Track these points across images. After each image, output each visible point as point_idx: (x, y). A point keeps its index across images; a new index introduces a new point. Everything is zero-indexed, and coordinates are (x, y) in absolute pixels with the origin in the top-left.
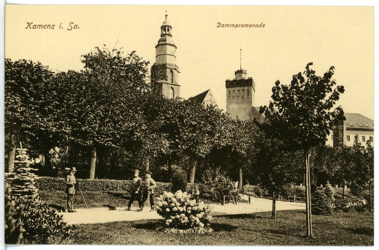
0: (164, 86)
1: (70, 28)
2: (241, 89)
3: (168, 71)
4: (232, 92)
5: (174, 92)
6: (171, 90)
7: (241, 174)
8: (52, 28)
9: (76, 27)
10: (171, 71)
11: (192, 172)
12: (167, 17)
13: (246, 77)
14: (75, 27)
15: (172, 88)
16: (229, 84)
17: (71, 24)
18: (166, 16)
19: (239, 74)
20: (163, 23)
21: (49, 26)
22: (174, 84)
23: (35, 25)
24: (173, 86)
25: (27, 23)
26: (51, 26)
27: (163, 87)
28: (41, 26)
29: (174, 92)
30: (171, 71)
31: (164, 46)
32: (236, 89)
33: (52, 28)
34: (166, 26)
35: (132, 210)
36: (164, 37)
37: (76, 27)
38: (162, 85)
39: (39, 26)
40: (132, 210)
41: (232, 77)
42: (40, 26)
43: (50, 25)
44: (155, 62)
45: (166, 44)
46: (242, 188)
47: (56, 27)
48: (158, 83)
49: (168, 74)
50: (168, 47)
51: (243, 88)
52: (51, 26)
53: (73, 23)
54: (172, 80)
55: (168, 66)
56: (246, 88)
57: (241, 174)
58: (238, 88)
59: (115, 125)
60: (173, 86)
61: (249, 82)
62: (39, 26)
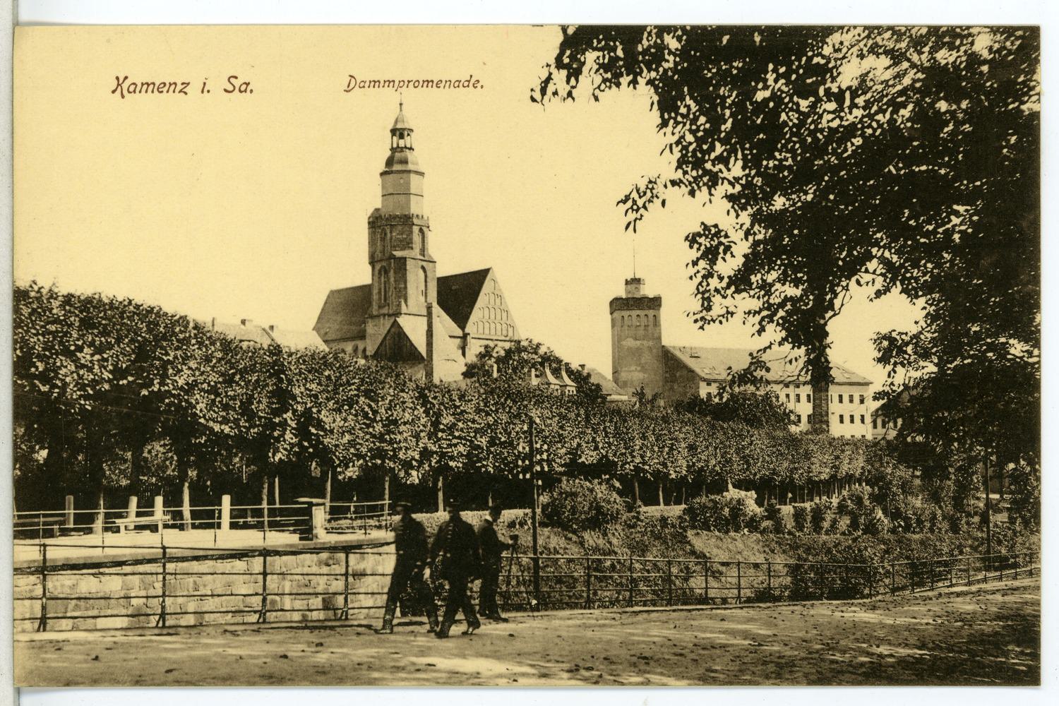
0: (410, 265)
1: (231, 88)
2: (642, 313)
3: (416, 229)
4: (626, 318)
5: (426, 276)
6: (421, 272)
8: (180, 91)
9: (245, 88)
10: (421, 231)
12: (403, 107)
13: (648, 291)
14: (243, 88)
15: (423, 268)
16: (617, 305)
17: (233, 80)
18: (401, 104)
19: (633, 286)
20: (396, 122)
21: (173, 86)
22: (426, 258)
23: (134, 84)
25: (596, 99)
27: (408, 267)
28: (151, 86)
30: (421, 231)
31: (405, 175)
32: (634, 313)
33: (180, 91)
34: (404, 129)
35: (452, 637)
36: (403, 154)
37: (245, 88)
38: (405, 264)
39: (145, 86)
40: (452, 637)
42: (148, 84)
44: (379, 206)
45: (409, 171)
47: (193, 90)
48: (394, 257)
49: (416, 238)
50: (413, 176)
51: (647, 312)
52: (179, 87)
53: (236, 78)
54: (423, 251)
55: (415, 221)
56: (651, 313)
58: (638, 312)
60: (424, 264)
61: (655, 303)
62: (145, 86)
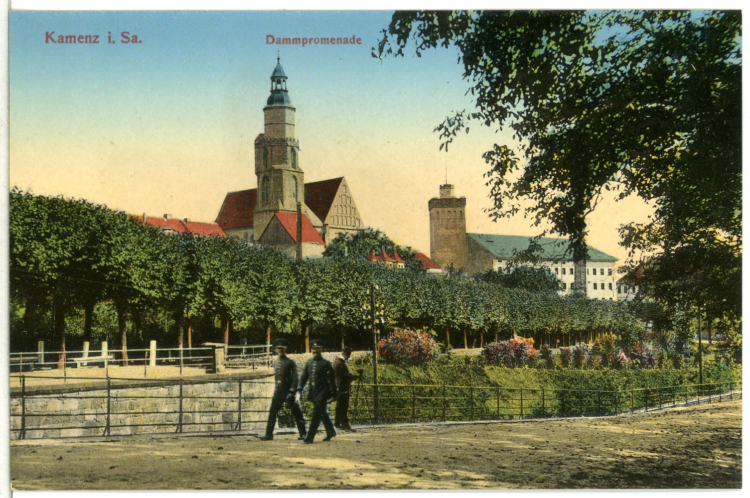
5: (296, 183)
7: (448, 334)
11: (240, 374)
15: (294, 177)
22: (297, 170)
24: (296, 174)
26: (93, 39)
29: (296, 183)
41: (437, 194)
43: (90, 36)
44: (263, 132)
45: (285, 107)
46: (633, 357)
48: (273, 169)
52: (93, 39)
55: (289, 143)
56: (458, 210)
57: (448, 334)
58: (450, 209)
59: (315, 296)
60: (296, 174)
